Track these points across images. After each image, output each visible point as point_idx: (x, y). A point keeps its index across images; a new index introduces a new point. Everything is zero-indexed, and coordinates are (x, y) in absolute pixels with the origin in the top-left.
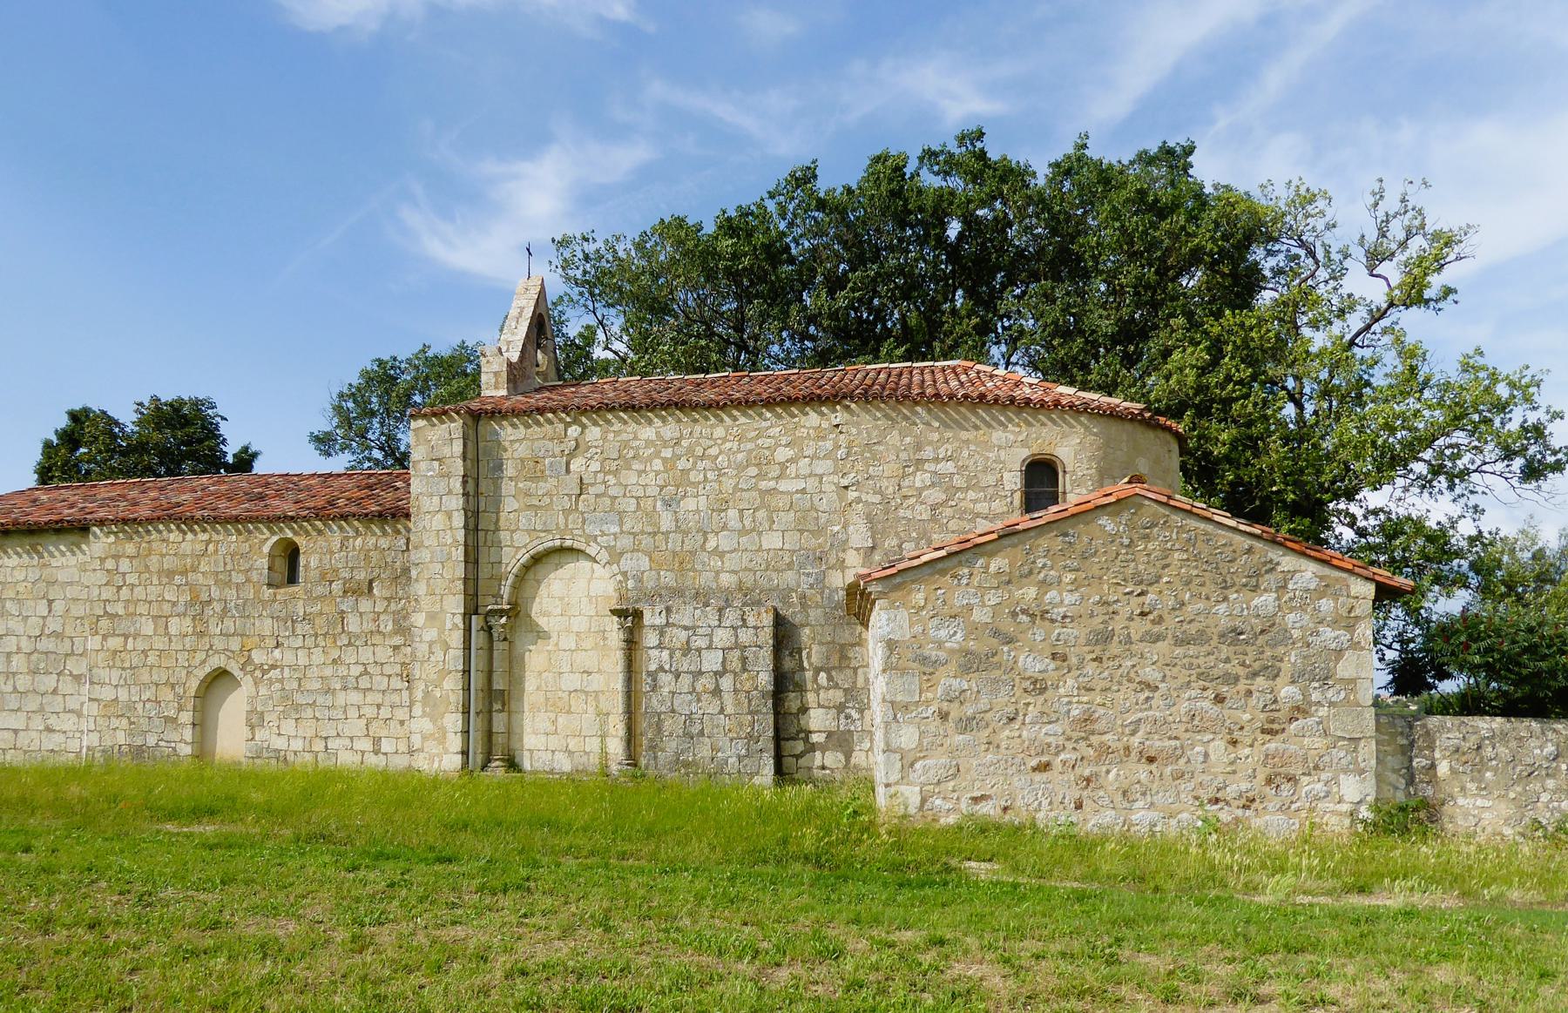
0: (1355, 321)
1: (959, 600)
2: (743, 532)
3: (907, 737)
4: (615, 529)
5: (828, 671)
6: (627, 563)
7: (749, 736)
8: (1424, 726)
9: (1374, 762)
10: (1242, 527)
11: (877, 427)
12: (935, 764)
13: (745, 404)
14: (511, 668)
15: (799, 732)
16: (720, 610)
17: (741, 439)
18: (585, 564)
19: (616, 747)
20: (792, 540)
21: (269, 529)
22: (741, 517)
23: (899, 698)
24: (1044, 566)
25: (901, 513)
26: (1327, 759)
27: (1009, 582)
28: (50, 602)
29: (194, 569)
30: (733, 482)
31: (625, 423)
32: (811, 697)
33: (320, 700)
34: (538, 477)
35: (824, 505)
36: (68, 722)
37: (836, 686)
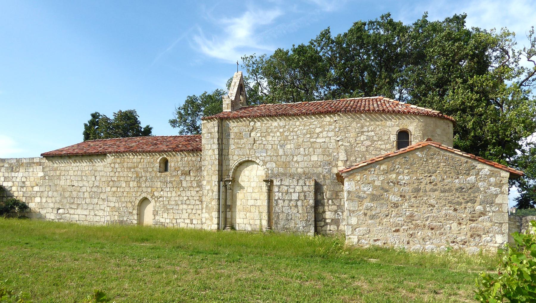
0: (523, 77)
1: (371, 178)
2: (305, 155)
3: (354, 221)
5: (332, 200)
6: (268, 165)
7: (307, 220)
8: (526, 219)
9: (507, 231)
10: (464, 155)
11: (349, 121)
12: (362, 229)
13: (306, 114)
14: (232, 198)
16: (298, 180)
17: (305, 125)
18: (255, 166)
19: (265, 223)
20: (321, 158)
21: (159, 155)
22: (305, 150)
24: (398, 168)
25: (356, 149)
26: (491, 229)
27: (387, 173)
28: (95, 177)
29: (137, 167)
30: (302, 139)
31: (268, 121)
32: (326, 208)
33: (175, 207)
34: (241, 138)
36: (101, 213)
37: (335, 204)
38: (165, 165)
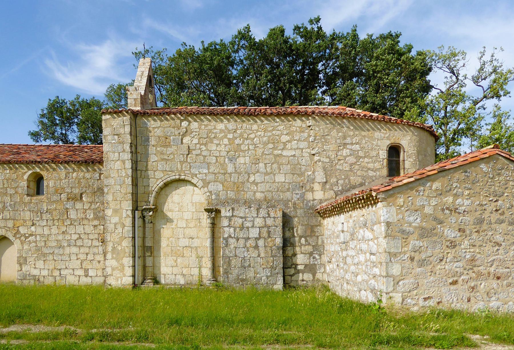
1: (419, 202)
2: (267, 174)
4: (205, 171)
5: (305, 238)
6: (211, 187)
7: (272, 267)
11: (327, 128)
12: (408, 283)
14: (154, 236)
15: (292, 265)
18: (190, 188)
19: (207, 272)
20: (289, 178)
21: (27, 167)
22: (266, 167)
23: (392, 251)
24: (456, 186)
25: (338, 167)
27: (441, 194)
30: (261, 150)
31: (210, 121)
32: (298, 249)
33: (56, 251)
34: (167, 145)
35: (303, 162)
37: (309, 244)
38: (38, 184)
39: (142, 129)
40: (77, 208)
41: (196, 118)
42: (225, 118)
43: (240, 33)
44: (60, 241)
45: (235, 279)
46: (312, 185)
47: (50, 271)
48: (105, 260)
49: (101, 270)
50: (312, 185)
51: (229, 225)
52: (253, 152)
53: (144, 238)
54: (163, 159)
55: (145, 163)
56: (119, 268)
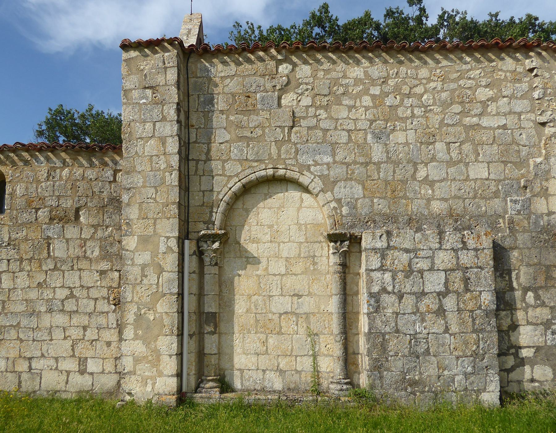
2: (451, 163)
4: (328, 159)
5: (535, 290)
6: (341, 191)
7: (475, 354)
14: (221, 291)
15: (509, 348)
18: (294, 194)
19: (330, 366)
20: (497, 171)
22: (449, 149)
30: (439, 118)
31: (334, 62)
32: (520, 315)
33: (24, 322)
37: (543, 305)
39: (200, 80)
40: (68, 236)
41: (308, 58)
42: (364, 57)
43: (313, 16)
44: (31, 301)
45: (397, 382)
46: (544, 183)
47: (10, 362)
48: (121, 340)
49: (112, 361)
50: (544, 183)
51: (382, 266)
52: (423, 121)
53: (201, 295)
54: (241, 138)
55: (205, 147)
56: (150, 358)
